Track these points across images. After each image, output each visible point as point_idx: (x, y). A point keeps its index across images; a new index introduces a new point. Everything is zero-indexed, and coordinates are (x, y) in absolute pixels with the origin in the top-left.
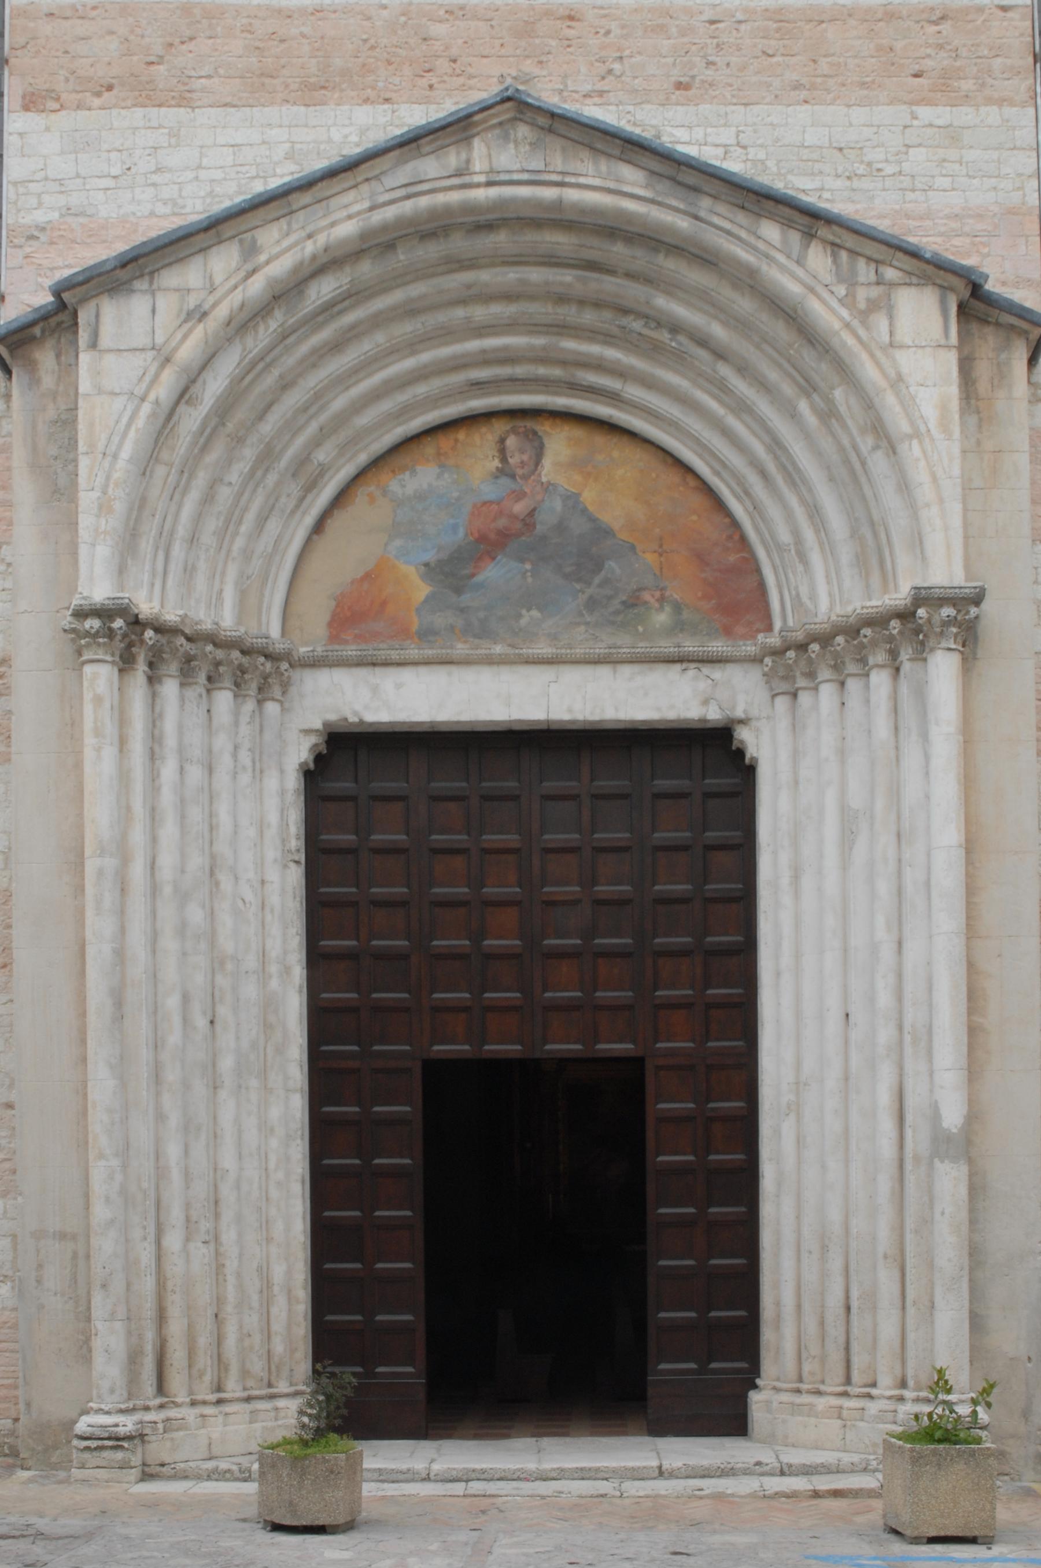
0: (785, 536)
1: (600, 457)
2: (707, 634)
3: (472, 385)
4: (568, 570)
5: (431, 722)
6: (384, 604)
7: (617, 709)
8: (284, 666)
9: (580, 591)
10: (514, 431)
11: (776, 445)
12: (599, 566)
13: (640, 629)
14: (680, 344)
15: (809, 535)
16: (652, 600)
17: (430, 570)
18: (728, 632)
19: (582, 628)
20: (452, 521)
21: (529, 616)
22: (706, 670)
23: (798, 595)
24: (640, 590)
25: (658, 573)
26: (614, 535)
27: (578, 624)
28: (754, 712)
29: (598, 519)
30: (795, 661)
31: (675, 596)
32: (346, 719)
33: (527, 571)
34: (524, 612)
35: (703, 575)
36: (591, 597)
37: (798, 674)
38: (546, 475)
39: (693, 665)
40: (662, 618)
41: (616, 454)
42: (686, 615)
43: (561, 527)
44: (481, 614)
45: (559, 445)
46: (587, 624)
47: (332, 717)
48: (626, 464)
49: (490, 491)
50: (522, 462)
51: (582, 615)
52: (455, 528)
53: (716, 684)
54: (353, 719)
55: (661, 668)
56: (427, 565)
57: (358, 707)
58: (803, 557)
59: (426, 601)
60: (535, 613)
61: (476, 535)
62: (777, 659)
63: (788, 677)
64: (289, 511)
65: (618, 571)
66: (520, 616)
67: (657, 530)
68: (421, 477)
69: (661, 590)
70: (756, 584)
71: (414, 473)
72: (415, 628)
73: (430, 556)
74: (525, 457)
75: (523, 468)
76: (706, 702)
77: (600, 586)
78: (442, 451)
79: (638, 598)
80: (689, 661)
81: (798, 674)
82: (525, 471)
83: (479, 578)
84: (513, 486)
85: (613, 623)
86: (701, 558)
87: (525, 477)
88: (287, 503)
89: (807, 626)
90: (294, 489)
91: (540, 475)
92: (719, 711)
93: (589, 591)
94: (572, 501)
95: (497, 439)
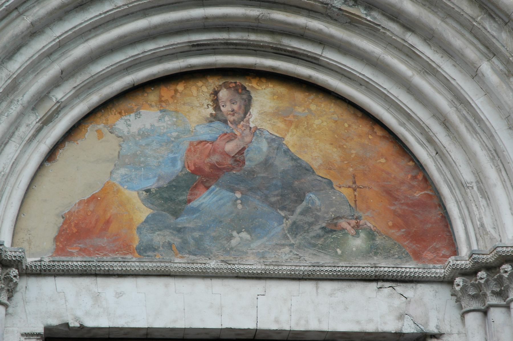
0: (466, 175)
1: (299, 110)
2: (399, 258)
3: (193, 46)
4: (273, 199)
5: (148, 328)
6: (108, 222)
7: (320, 321)
8: (14, 272)
9: (284, 217)
10: (226, 86)
11: (459, 99)
12: (300, 198)
13: (339, 251)
14: (375, 18)
15: (492, 173)
16: (349, 228)
17: (150, 196)
18: (417, 256)
19: (287, 249)
20: (171, 155)
21: (239, 238)
22: (400, 288)
23: (482, 225)
24: (338, 218)
25: (353, 205)
26: (313, 172)
27: (283, 245)
28: (445, 328)
29: (299, 159)
30: (487, 281)
31: (369, 225)
32: (67, 324)
33: (237, 199)
34: (235, 233)
35: (392, 208)
36: (294, 223)
37: (489, 293)
38: (253, 122)
39: (387, 284)
40: (358, 243)
41: (313, 107)
42: (379, 241)
43: (267, 164)
44: (197, 234)
45: (265, 98)
46: (292, 245)
47: (54, 322)
48: (323, 115)
49: (205, 133)
50: (233, 111)
51: (288, 238)
52: (174, 161)
53: (409, 302)
54: (74, 324)
55: (360, 285)
56: (148, 191)
57: (79, 313)
58: (485, 193)
59: (146, 221)
60: (244, 235)
61: (193, 168)
62: (467, 280)
63: (479, 296)
64: (27, 138)
65: (318, 202)
66: (231, 237)
67: (351, 169)
68: (144, 119)
69: (356, 219)
70: (439, 217)
71: (138, 115)
72: (136, 244)
73: (152, 184)
74: (235, 107)
75: (233, 115)
76: (401, 317)
77: (302, 214)
78: (163, 99)
79: (336, 225)
80: (384, 280)
81: (489, 293)
82: (236, 117)
83: (195, 204)
84: (225, 130)
85: (314, 245)
86: (390, 194)
87: (236, 123)
88: (25, 130)
89: (499, 249)
90: (33, 120)
91: (248, 121)
92: (413, 326)
93: (292, 218)
94: (277, 143)
95: (211, 91)
